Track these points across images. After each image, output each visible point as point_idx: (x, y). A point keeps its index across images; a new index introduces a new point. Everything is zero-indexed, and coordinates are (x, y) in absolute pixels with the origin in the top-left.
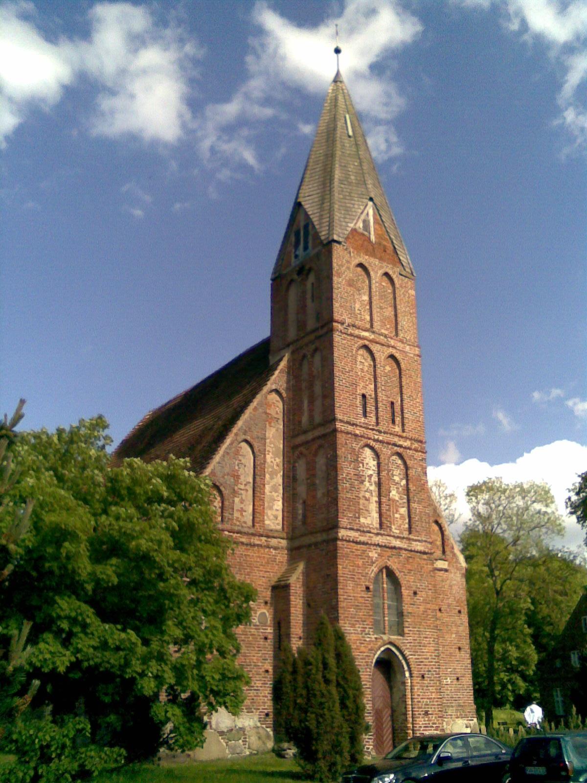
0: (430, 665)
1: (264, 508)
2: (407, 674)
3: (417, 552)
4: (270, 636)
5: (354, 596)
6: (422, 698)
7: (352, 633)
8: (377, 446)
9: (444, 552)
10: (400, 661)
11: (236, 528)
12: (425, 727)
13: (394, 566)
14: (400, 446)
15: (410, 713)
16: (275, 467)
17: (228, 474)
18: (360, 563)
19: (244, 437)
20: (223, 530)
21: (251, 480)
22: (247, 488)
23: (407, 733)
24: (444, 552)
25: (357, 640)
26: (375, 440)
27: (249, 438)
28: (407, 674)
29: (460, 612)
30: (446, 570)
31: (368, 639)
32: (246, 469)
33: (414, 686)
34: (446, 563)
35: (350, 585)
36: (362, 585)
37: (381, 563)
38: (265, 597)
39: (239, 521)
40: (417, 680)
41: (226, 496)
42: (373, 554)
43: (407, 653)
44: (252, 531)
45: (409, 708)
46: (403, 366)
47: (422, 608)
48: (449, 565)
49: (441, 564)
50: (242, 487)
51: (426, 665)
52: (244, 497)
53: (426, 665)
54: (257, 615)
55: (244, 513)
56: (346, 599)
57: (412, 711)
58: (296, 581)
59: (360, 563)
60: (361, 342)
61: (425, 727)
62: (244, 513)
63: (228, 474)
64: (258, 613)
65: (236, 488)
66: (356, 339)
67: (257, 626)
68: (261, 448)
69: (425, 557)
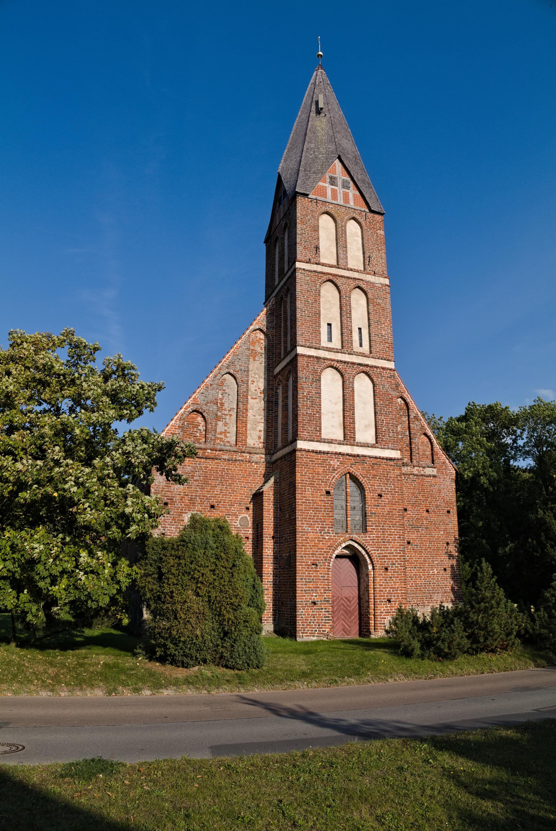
0: (395, 559)
1: (246, 429)
2: (370, 567)
3: (383, 459)
4: (251, 537)
5: (312, 500)
6: (384, 588)
7: (310, 532)
8: (340, 366)
9: (433, 461)
10: (363, 556)
11: (219, 447)
12: (386, 612)
13: (357, 472)
14: (367, 366)
15: (373, 600)
16: (75, 358)
17: (211, 402)
18: (321, 470)
19: (227, 370)
20: (206, 449)
21: (235, 407)
22: (230, 413)
23: (369, 618)
24: (433, 461)
25: (315, 538)
26: (338, 361)
27: (232, 371)
28: (370, 567)
29: (448, 512)
30: (434, 476)
31: (327, 538)
32: (230, 397)
33: (376, 577)
34: (435, 470)
35: (309, 491)
36: (322, 490)
37: (342, 470)
38: (246, 504)
39: (223, 441)
40: (380, 572)
41: (209, 421)
42: (335, 463)
43: (369, 548)
44: (235, 449)
45: (372, 596)
46: (370, 296)
47: (387, 509)
48: (438, 472)
49: (429, 471)
50: (226, 412)
51: (390, 559)
52: (227, 421)
53: (390, 559)
54: (239, 519)
55: (228, 435)
56: (304, 502)
57: (374, 599)
58: (269, 489)
59: (321, 470)
60: (325, 278)
61: (386, 612)
62: (228, 435)
63: (211, 402)
64: (240, 518)
65: (219, 414)
66: (320, 275)
67: (239, 528)
68: (245, 379)
69: (392, 463)
